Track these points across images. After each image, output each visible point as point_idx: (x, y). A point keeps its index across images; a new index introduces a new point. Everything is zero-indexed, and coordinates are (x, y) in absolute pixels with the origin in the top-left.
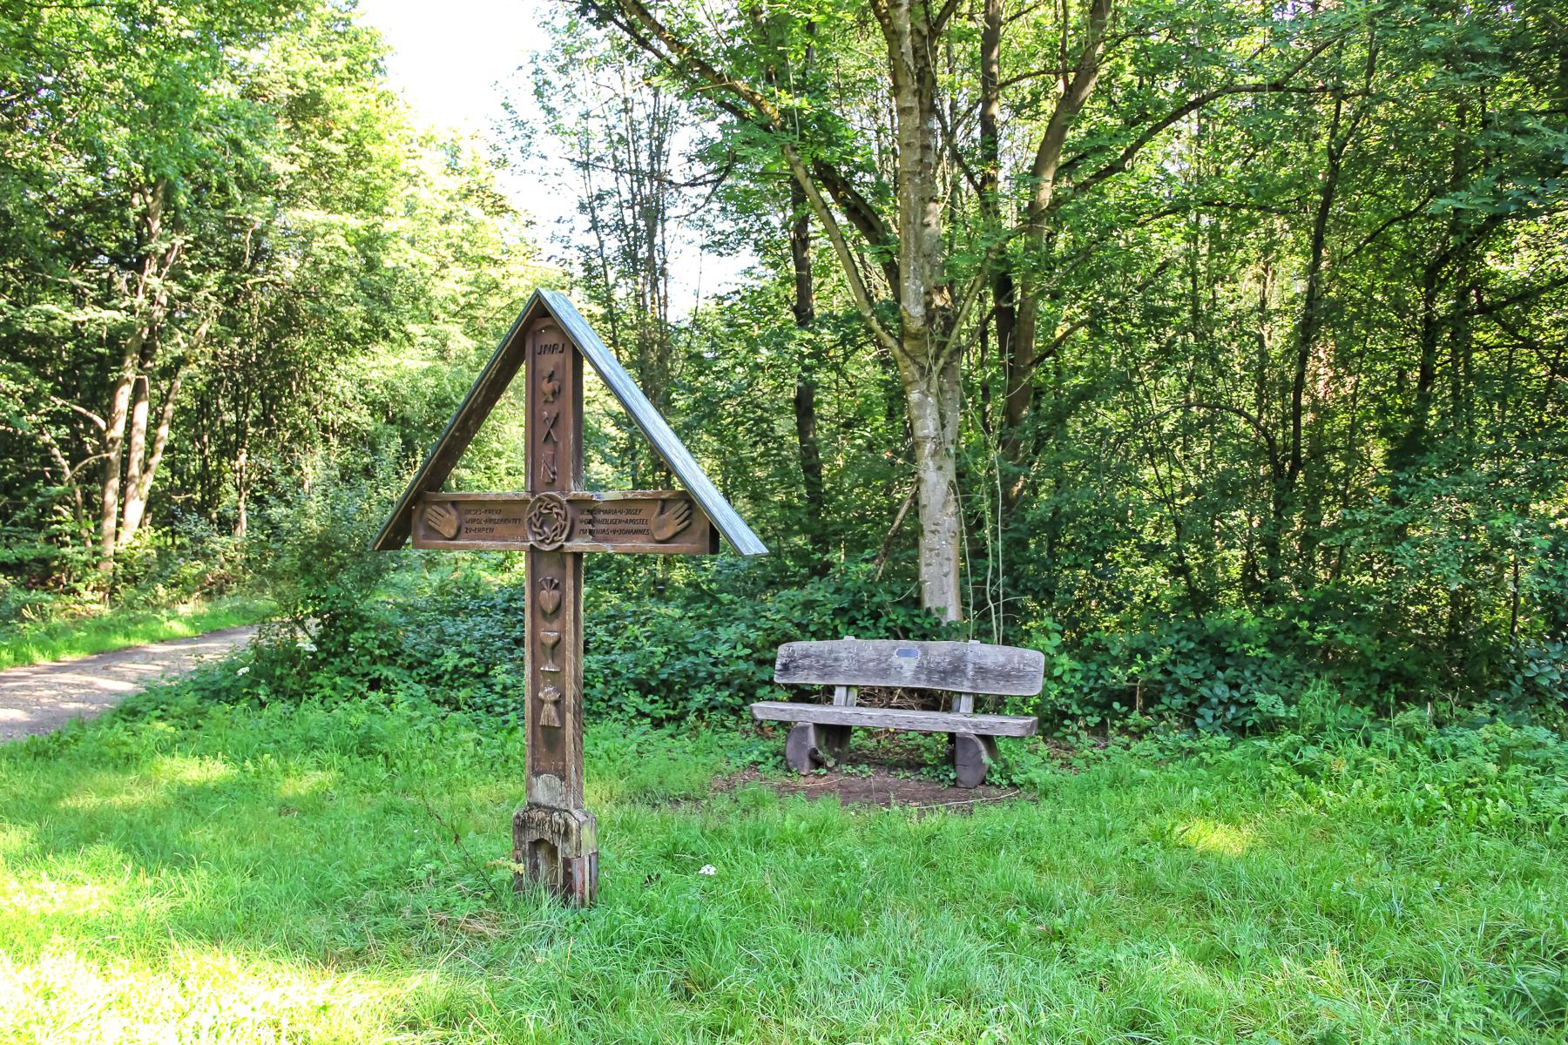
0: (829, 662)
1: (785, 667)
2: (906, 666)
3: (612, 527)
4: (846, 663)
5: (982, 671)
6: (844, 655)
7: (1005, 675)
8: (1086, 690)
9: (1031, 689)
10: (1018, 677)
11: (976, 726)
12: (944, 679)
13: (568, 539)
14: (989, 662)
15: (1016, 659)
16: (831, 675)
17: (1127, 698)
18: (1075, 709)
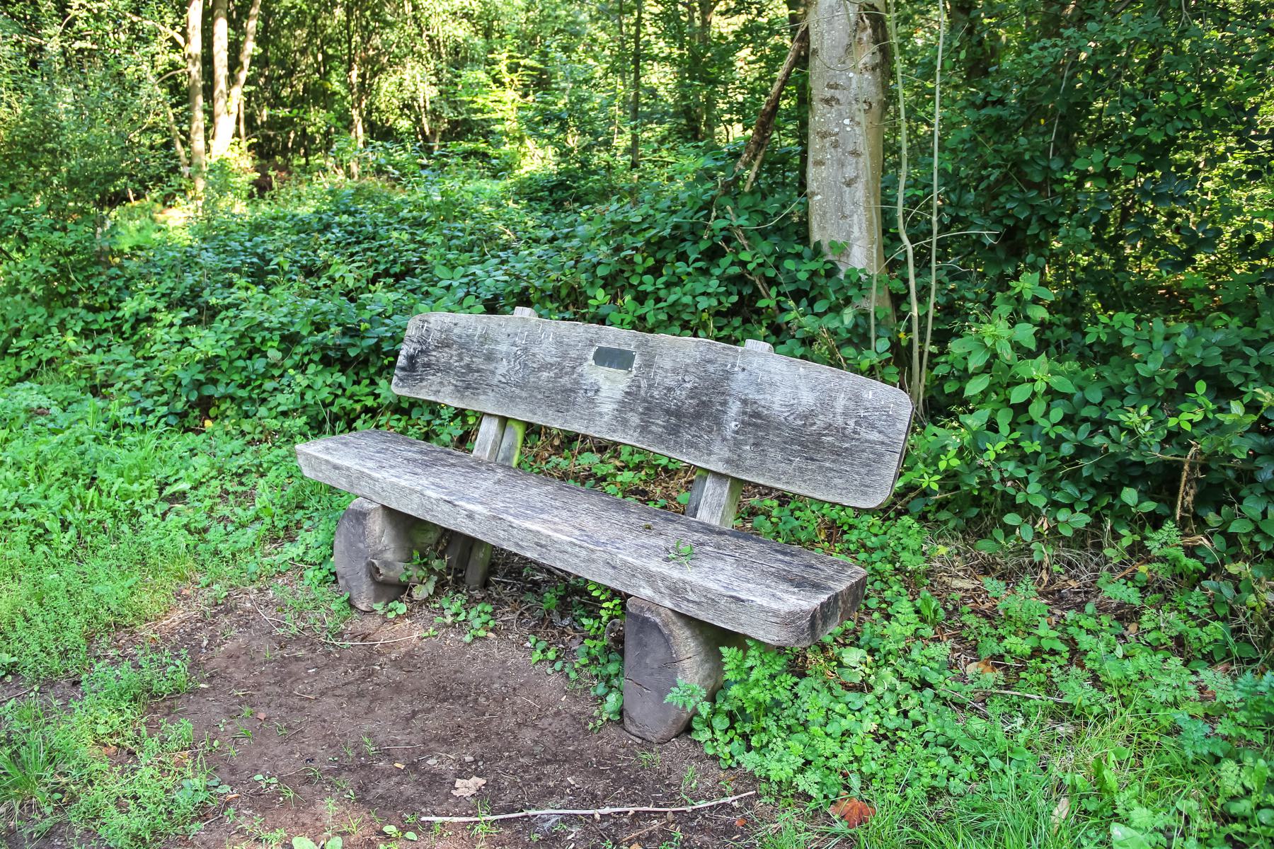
0: (478, 362)
2: (605, 386)
4: (502, 367)
5: (756, 420)
8: (1067, 449)
9: (864, 489)
10: (837, 453)
11: (676, 590)
12: (674, 431)
14: (776, 403)
15: (841, 403)
17: (1162, 482)
18: (1034, 494)
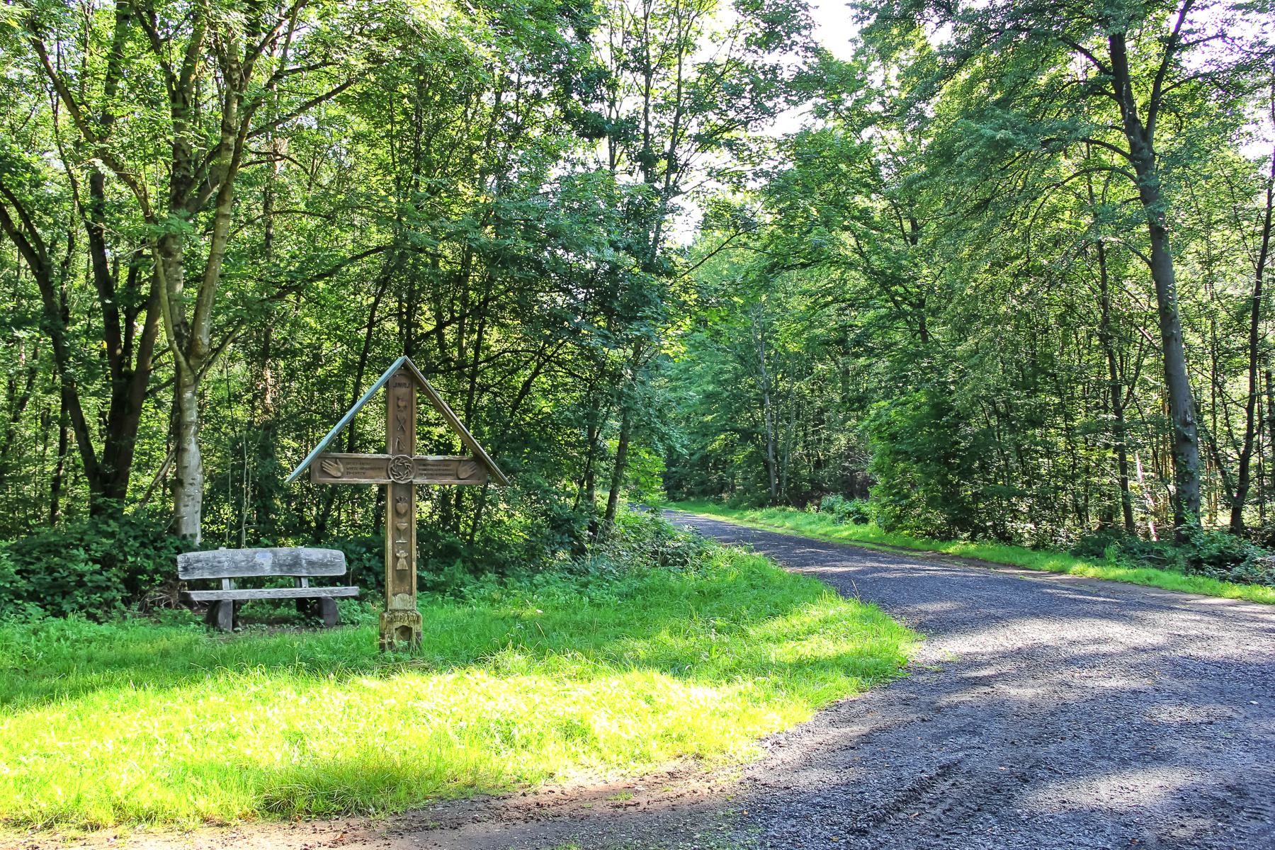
1: (185, 569)
6: (223, 559)
7: (324, 565)
14: (314, 558)
16: (218, 572)
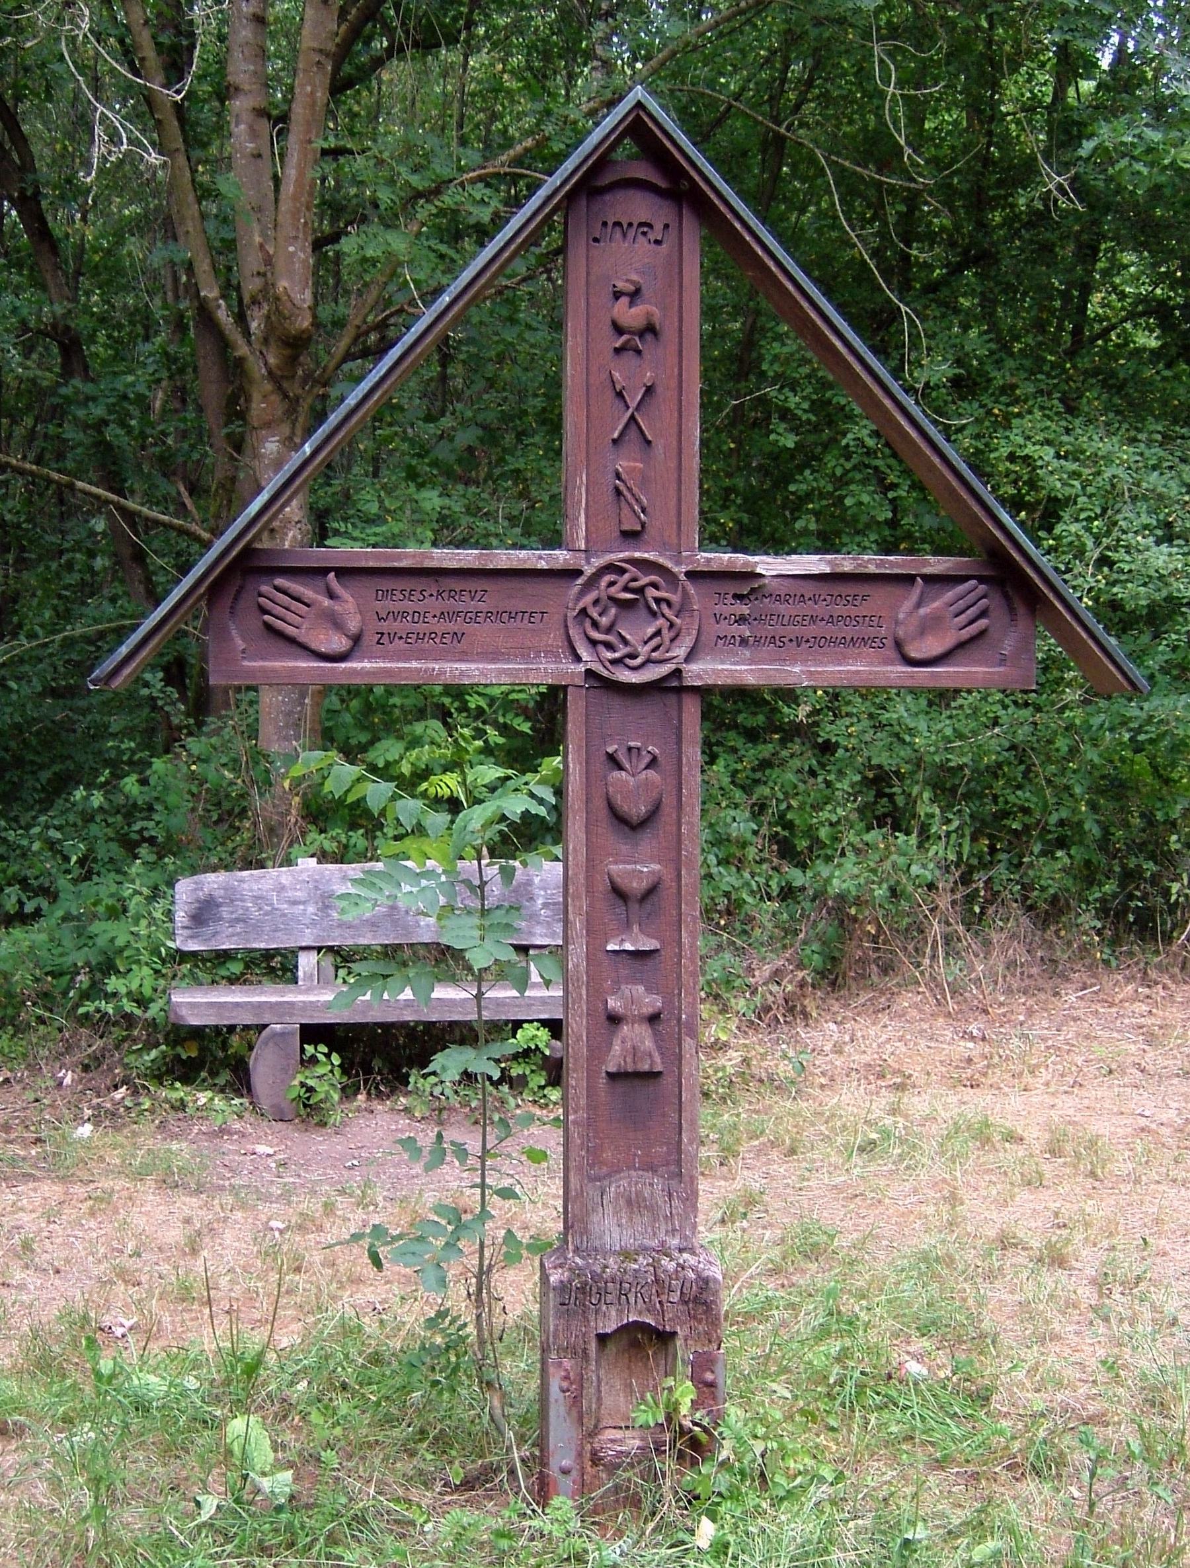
3: (793, 631)
13: (688, 659)
